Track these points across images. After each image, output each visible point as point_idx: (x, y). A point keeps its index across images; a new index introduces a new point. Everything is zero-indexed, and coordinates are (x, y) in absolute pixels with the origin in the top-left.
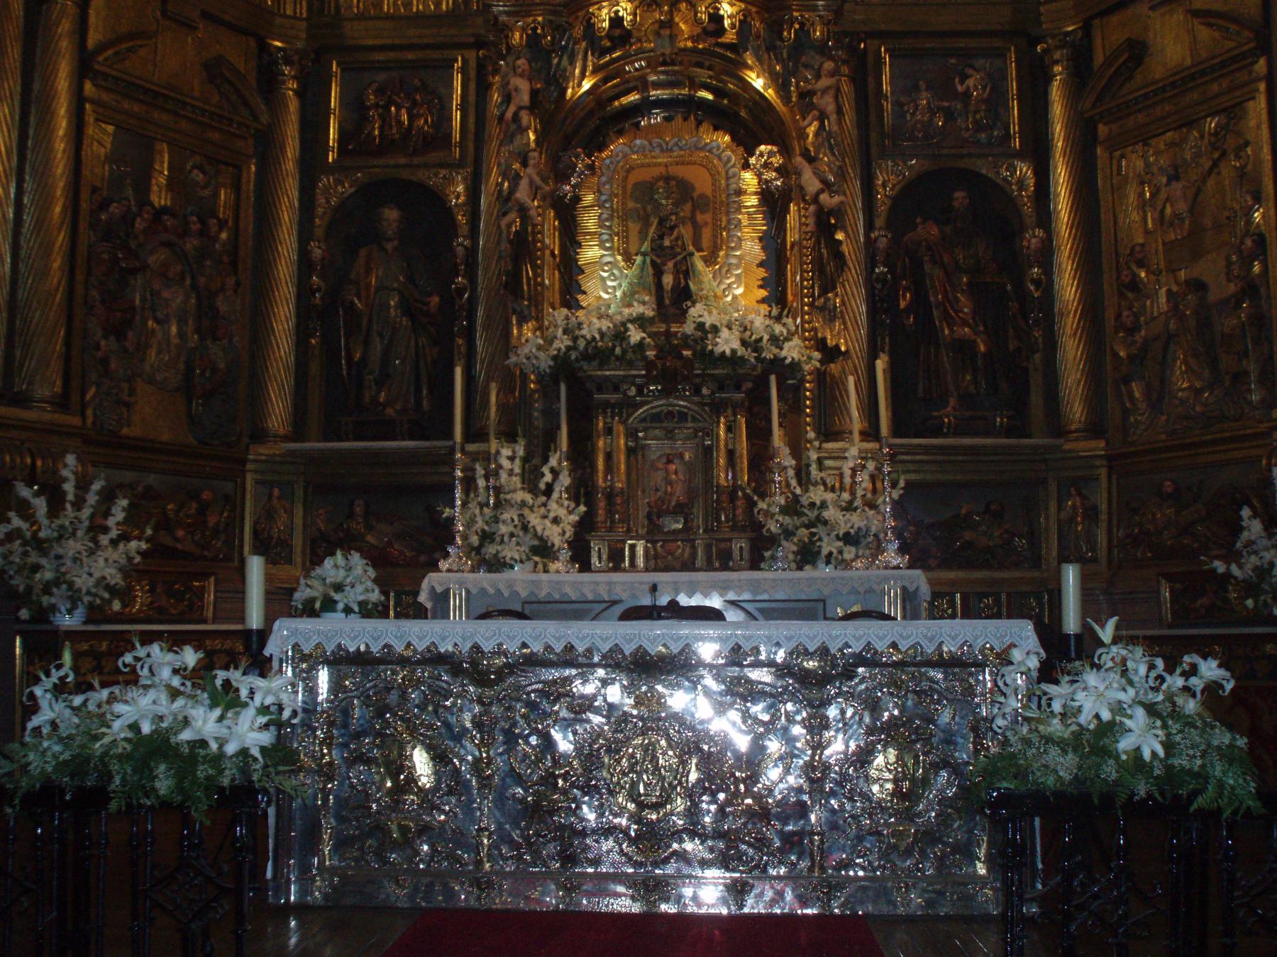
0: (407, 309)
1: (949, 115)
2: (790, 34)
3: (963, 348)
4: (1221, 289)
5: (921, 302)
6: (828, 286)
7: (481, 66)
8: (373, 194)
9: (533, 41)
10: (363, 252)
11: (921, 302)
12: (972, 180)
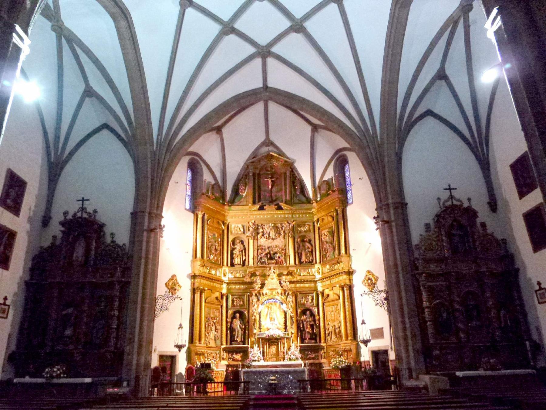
0: (240, 327)
1: (307, 301)
2: (287, 294)
3: (309, 332)
4: (337, 327)
5: (303, 327)
6: (292, 325)
7: (249, 296)
8: (235, 313)
9: (256, 295)
10: (234, 320)
11: (303, 327)
12: (310, 310)
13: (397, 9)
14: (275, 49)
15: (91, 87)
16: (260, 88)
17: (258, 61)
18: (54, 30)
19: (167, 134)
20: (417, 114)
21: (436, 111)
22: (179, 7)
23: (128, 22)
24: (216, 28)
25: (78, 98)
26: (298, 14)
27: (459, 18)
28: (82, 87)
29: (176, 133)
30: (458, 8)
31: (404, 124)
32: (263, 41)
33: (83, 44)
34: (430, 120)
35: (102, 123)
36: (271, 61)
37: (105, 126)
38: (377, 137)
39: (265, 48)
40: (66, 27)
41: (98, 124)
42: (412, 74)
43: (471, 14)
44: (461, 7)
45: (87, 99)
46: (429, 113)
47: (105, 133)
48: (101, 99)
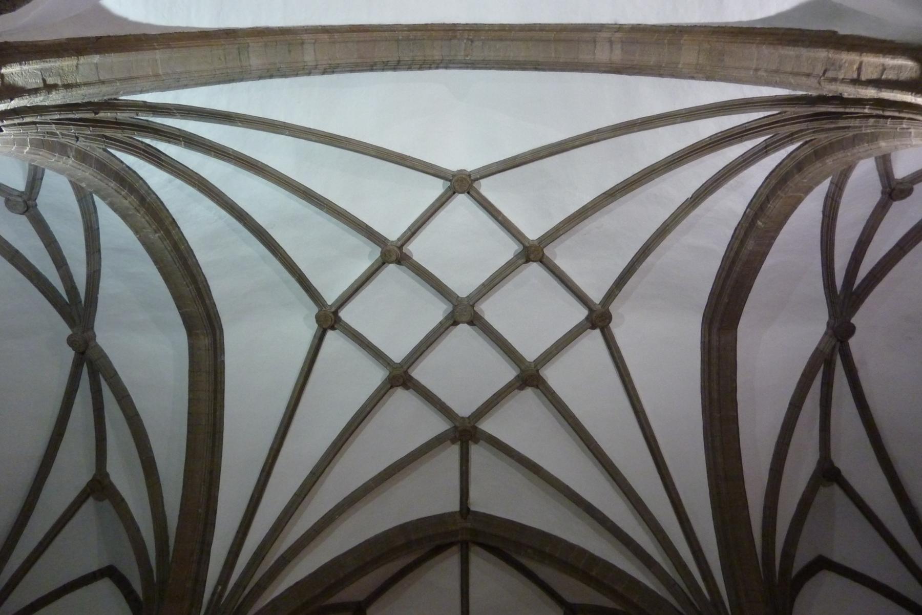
13: (715, 331)
14: (488, 426)
15: (107, 475)
16: (456, 512)
17: (453, 452)
18: (71, 342)
19: (240, 585)
20: (799, 563)
21: (837, 558)
22: (316, 326)
23: (215, 340)
24: (377, 375)
25: (94, 567)
26: (531, 352)
27: (832, 354)
28: (84, 475)
29: (261, 587)
30: (826, 333)
31: (777, 574)
32: (464, 408)
33: (119, 380)
34: (828, 581)
35: (106, 563)
36: (478, 453)
37: (110, 573)
38: (723, 603)
39: (467, 421)
40: (97, 345)
41: (94, 566)
42: (768, 467)
43: (853, 342)
44: (830, 331)
45: (90, 502)
46: (822, 564)
47: (105, 586)
48: (119, 503)
